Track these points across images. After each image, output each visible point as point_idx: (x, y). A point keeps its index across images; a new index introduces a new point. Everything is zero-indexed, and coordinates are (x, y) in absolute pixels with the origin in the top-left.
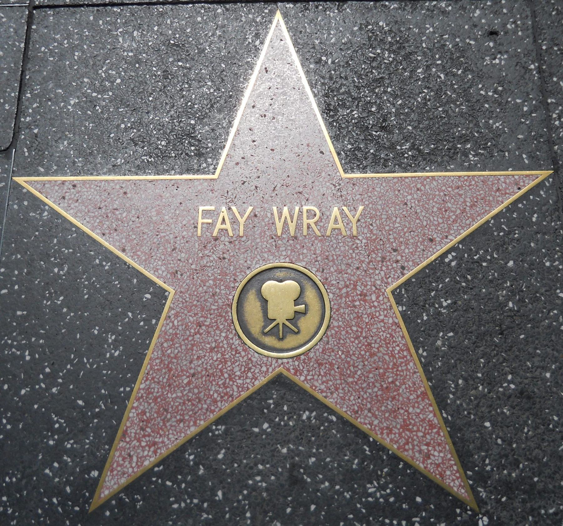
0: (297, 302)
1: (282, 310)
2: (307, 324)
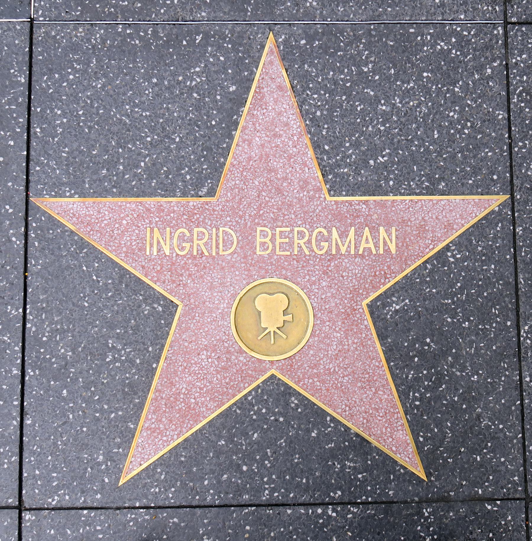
0: (285, 312)
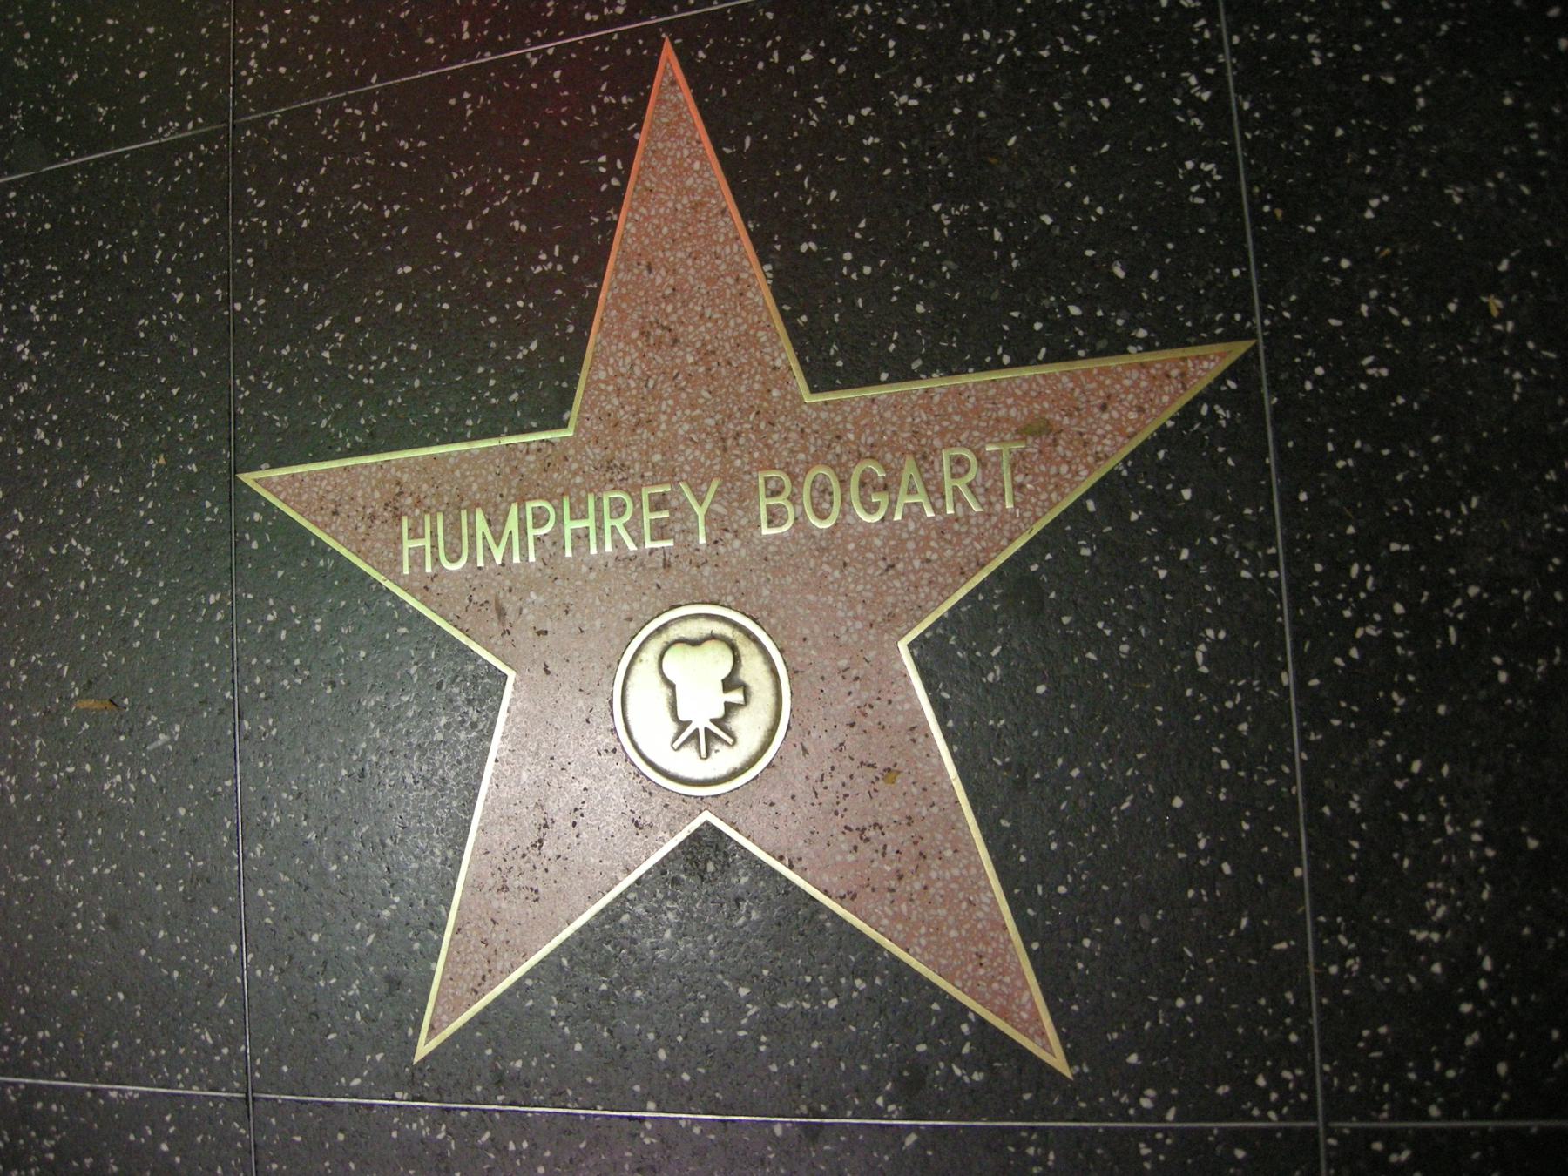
0: (729, 683)
1: (703, 705)
2: (750, 727)
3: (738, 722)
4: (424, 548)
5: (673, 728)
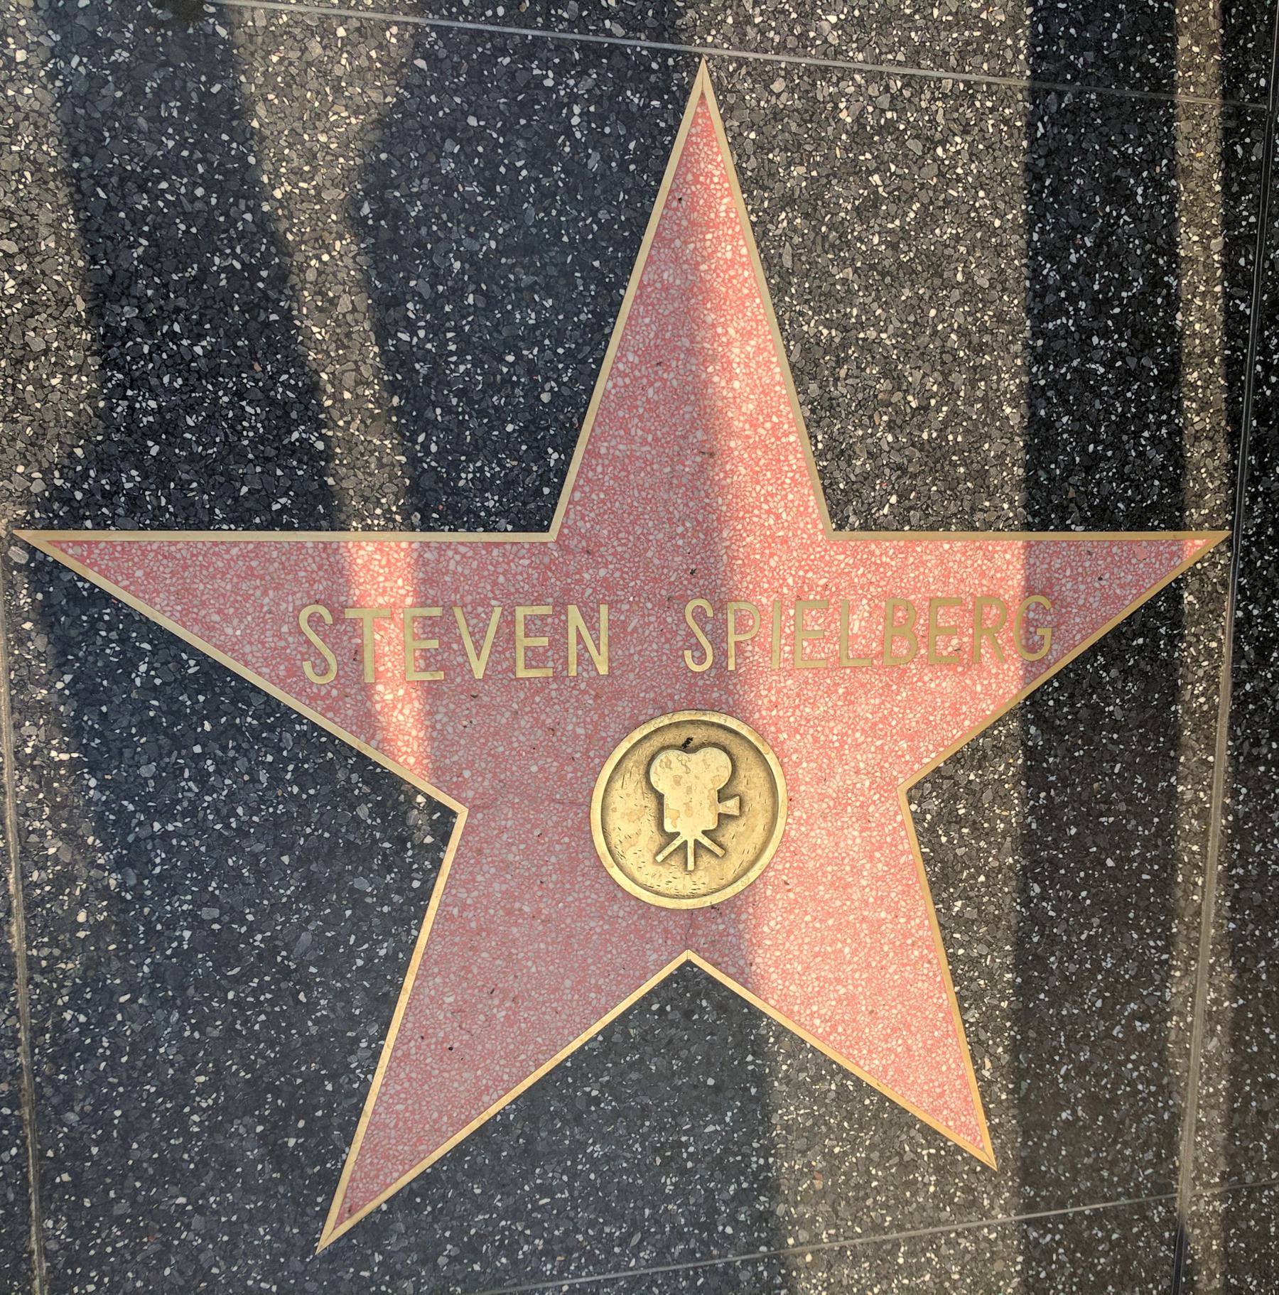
0: (723, 795)
1: (690, 824)
3: (728, 835)
4: (526, 635)
5: (659, 840)
